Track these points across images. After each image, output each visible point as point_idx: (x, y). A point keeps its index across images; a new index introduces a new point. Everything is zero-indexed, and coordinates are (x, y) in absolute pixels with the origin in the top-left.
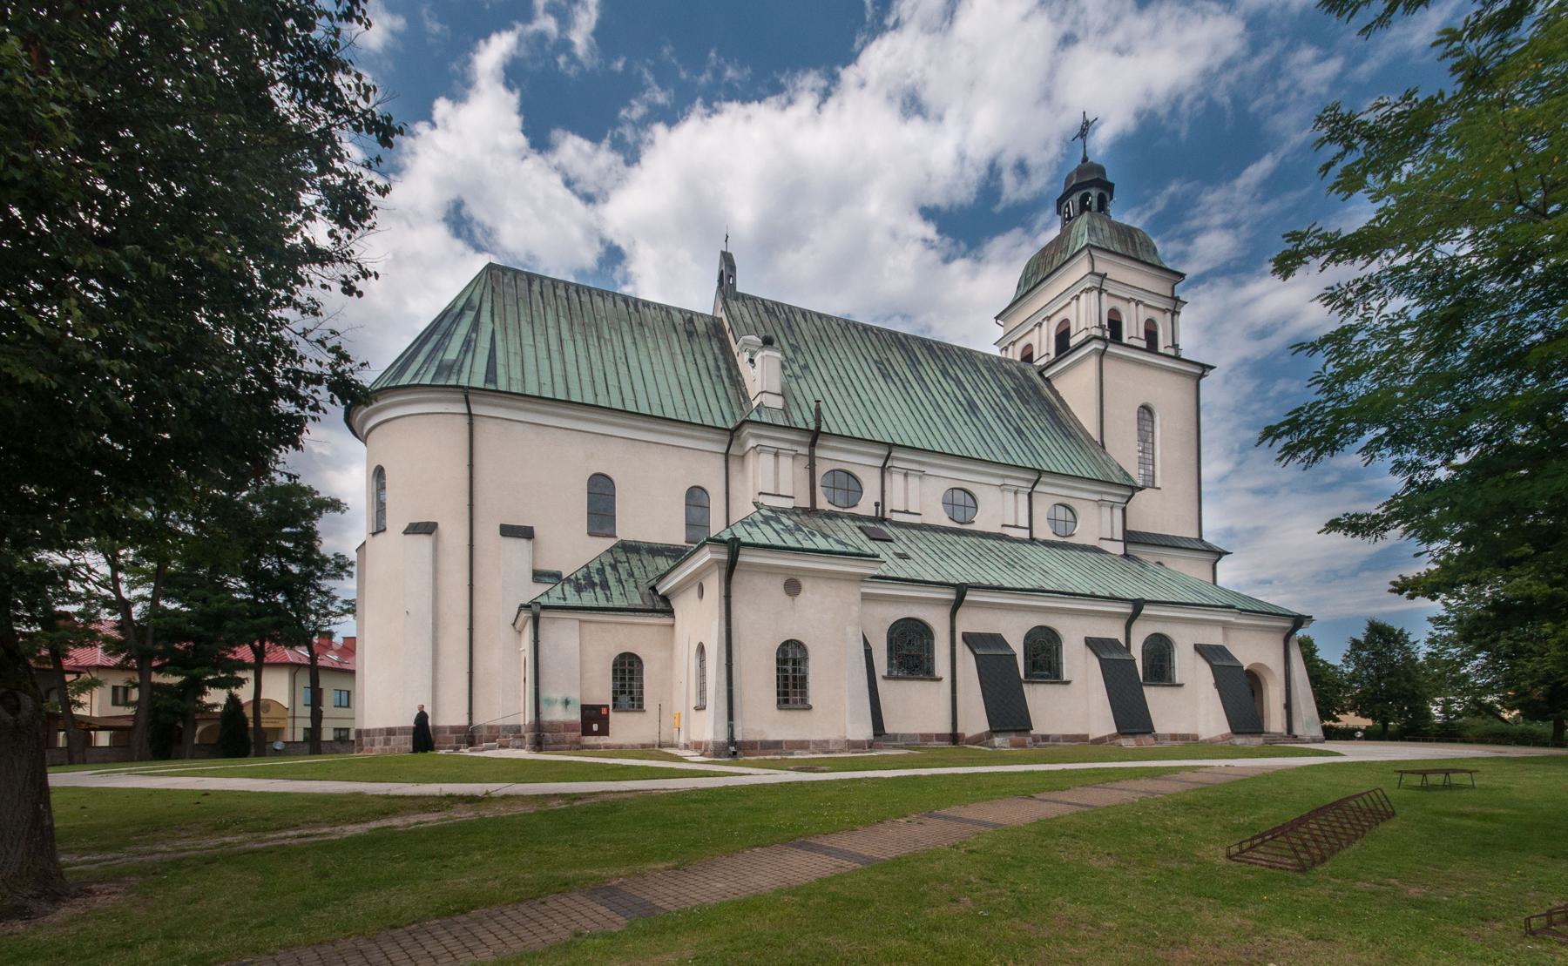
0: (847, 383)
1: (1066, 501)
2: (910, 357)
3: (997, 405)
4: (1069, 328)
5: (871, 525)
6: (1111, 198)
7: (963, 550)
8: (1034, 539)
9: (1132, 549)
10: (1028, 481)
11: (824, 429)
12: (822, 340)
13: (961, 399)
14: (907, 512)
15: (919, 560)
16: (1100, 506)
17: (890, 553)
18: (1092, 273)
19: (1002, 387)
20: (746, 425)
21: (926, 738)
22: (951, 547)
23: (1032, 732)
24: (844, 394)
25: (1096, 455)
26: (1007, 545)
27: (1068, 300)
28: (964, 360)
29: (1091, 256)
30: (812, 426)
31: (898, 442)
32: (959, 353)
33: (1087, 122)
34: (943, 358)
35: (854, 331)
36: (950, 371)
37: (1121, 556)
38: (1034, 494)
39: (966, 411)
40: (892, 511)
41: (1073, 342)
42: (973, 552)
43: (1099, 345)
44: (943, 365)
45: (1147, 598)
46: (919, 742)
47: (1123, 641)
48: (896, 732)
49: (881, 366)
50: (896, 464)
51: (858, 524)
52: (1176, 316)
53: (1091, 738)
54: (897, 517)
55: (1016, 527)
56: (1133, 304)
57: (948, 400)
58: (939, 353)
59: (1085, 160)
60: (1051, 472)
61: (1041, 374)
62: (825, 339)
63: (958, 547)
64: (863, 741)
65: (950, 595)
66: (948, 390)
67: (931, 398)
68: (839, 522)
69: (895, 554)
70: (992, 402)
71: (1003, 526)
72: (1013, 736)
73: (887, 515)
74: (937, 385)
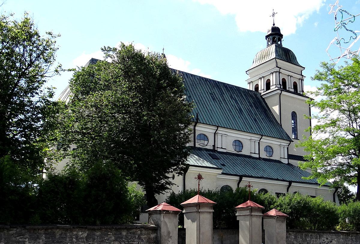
2: (220, 91)
3: (248, 109)
7: (239, 162)
8: (260, 158)
12: (193, 85)
13: (237, 108)
14: (222, 148)
17: (219, 164)
18: (277, 67)
19: (249, 102)
25: (279, 128)
26: (252, 160)
28: (237, 91)
29: (276, 61)
32: (235, 88)
34: (231, 91)
35: (202, 81)
36: (233, 97)
39: (239, 112)
40: (217, 147)
45: (293, 180)
49: (212, 95)
55: (255, 153)
56: (289, 77)
57: (233, 108)
58: (229, 89)
62: (194, 85)
63: (238, 161)
65: (287, 184)
66: (233, 104)
67: (228, 107)
69: (221, 164)
70: (247, 109)
74: (229, 102)
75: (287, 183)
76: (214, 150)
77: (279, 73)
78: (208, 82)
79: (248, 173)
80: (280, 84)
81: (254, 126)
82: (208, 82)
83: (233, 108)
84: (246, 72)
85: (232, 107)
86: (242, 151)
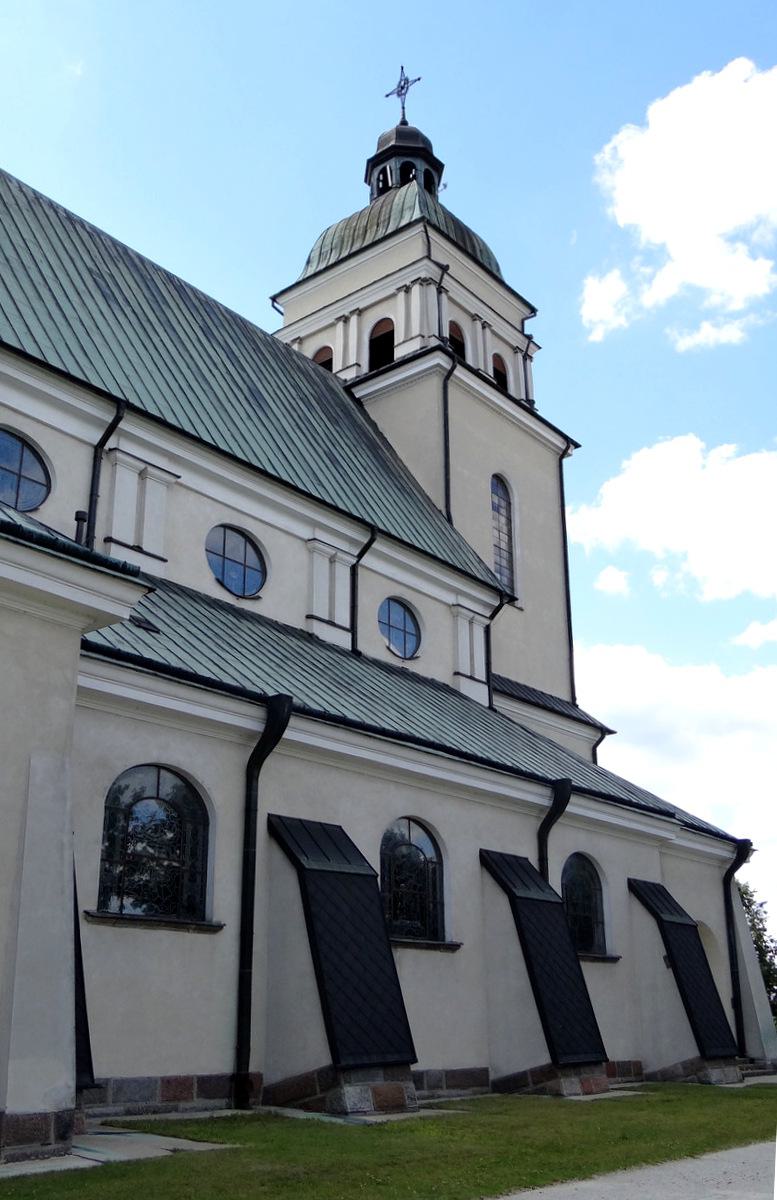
1: (408, 596)
4: (392, 332)
9: (501, 703)
10: (352, 541)
14: (138, 549)
16: (455, 616)
18: (428, 257)
21: (176, 1088)
23: (414, 1068)
27: (392, 290)
38: (360, 571)
40: (109, 540)
41: (399, 353)
44: (203, 320)
46: (157, 1102)
47: (534, 861)
48: (109, 1076)
50: (126, 446)
52: (528, 361)
53: (492, 1076)
54: (118, 554)
55: (331, 623)
56: (479, 324)
59: (404, 122)
64: (44, 1116)
71: (309, 617)
72: (380, 1082)
73: (99, 548)
75: (541, 795)
77: (440, 290)
84: (274, 299)
86: (259, 598)
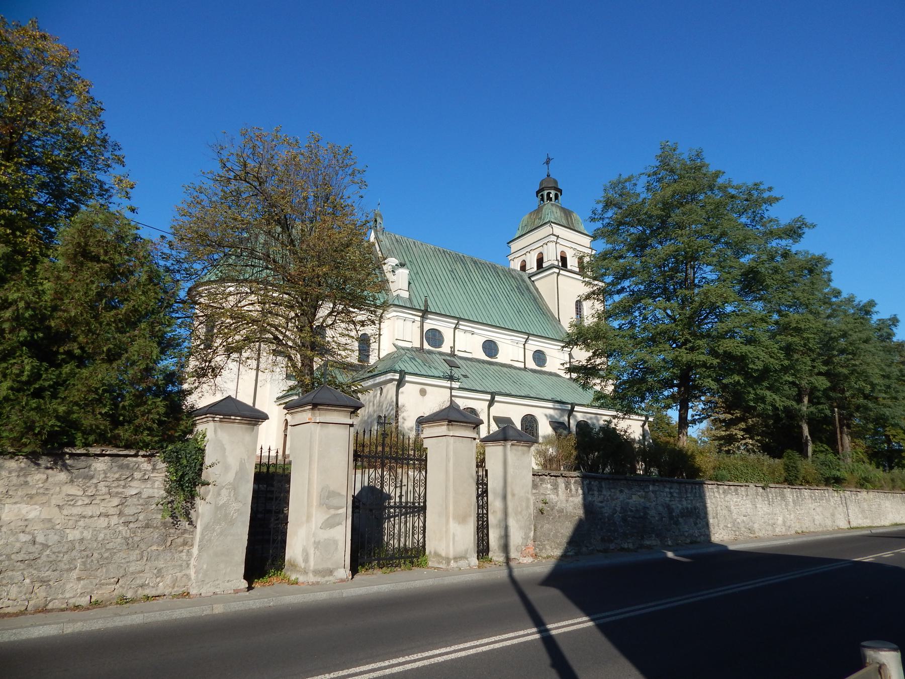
0: (437, 283)
5: (449, 358)
6: (561, 195)
7: (492, 374)
11: (429, 310)
14: (465, 352)
15: (473, 379)
20: (392, 306)
22: (487, 372)
24: (436, 289)
26: (513, 371)
30: (423, 308)
31: (462, 317)
33: (549, 159)
37: (568, 379)
41: (544, 265)
42: (497, 374)
43: (557, 270)
51: (443, 357)
57: (484, 293)
60: (534, 335)
61: (529, 278)
65: (489, 397)
66: (485, 287)
68: (434, 355)
73: (456, 353)
76: (453, 354)
78: (447, 255)
79: (505, 389)
80: (557, 260)
81: (517, 320)
82: (447, 255)
83: (484, 293)
85: (483, 291)
